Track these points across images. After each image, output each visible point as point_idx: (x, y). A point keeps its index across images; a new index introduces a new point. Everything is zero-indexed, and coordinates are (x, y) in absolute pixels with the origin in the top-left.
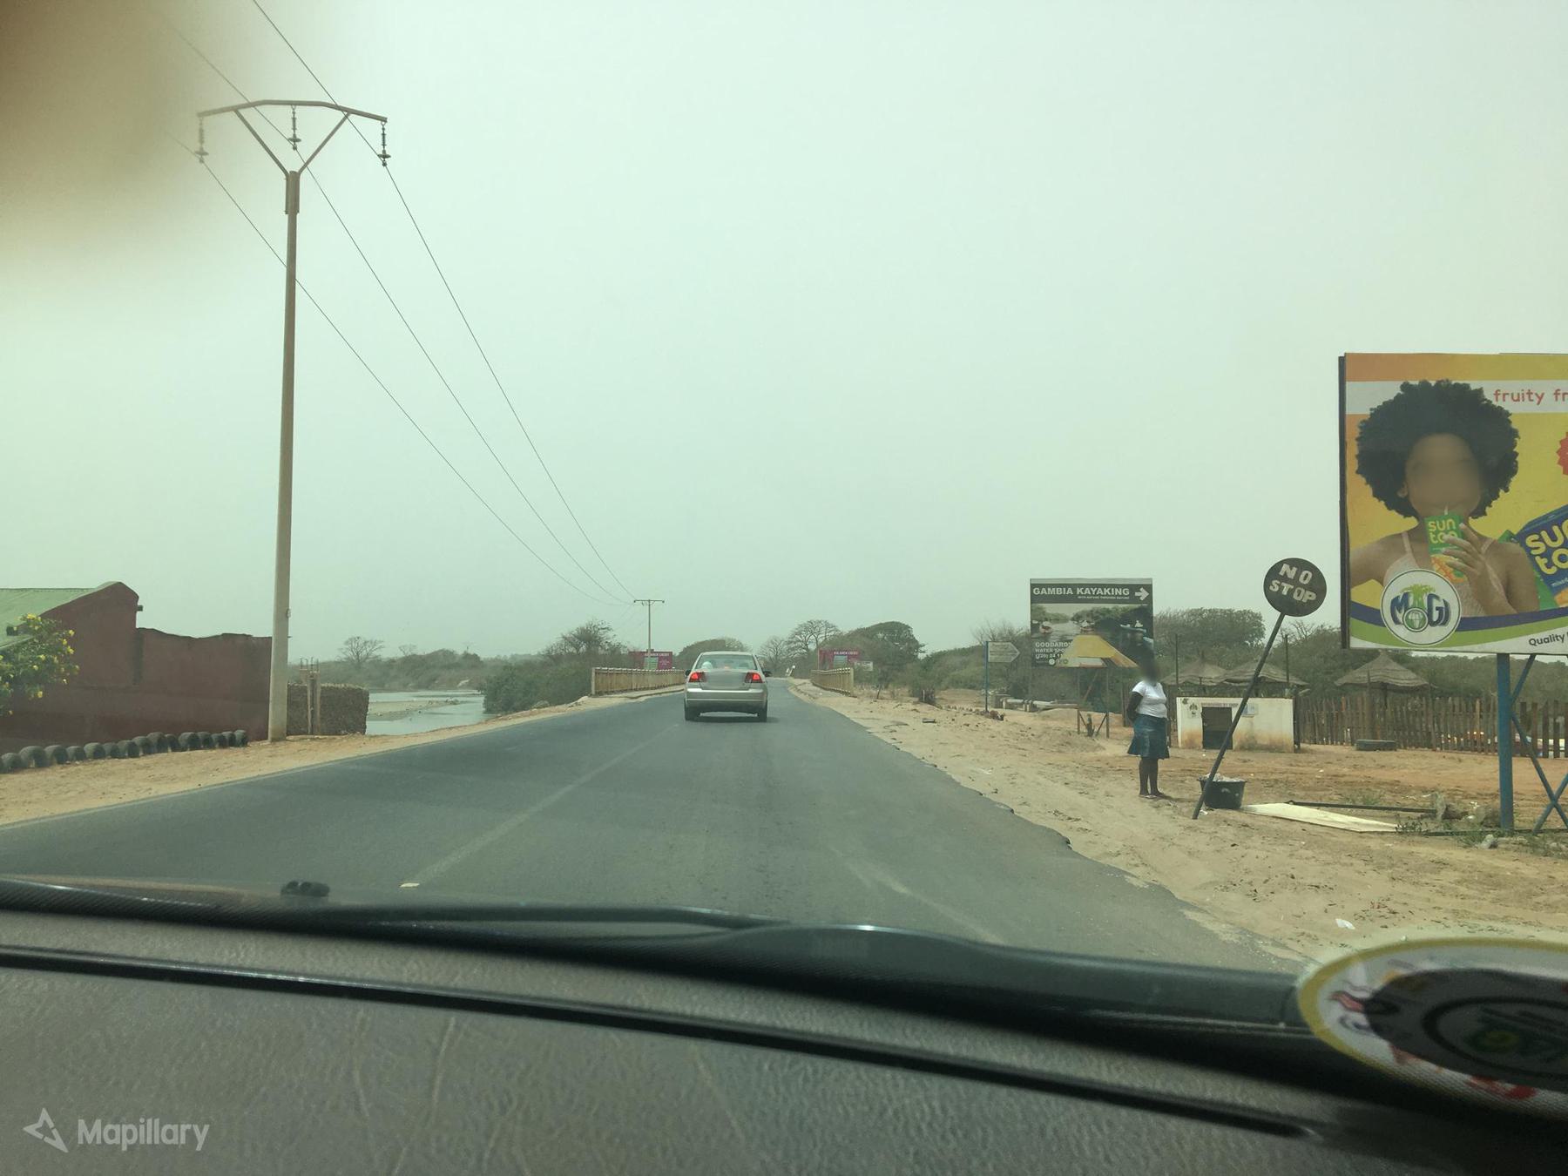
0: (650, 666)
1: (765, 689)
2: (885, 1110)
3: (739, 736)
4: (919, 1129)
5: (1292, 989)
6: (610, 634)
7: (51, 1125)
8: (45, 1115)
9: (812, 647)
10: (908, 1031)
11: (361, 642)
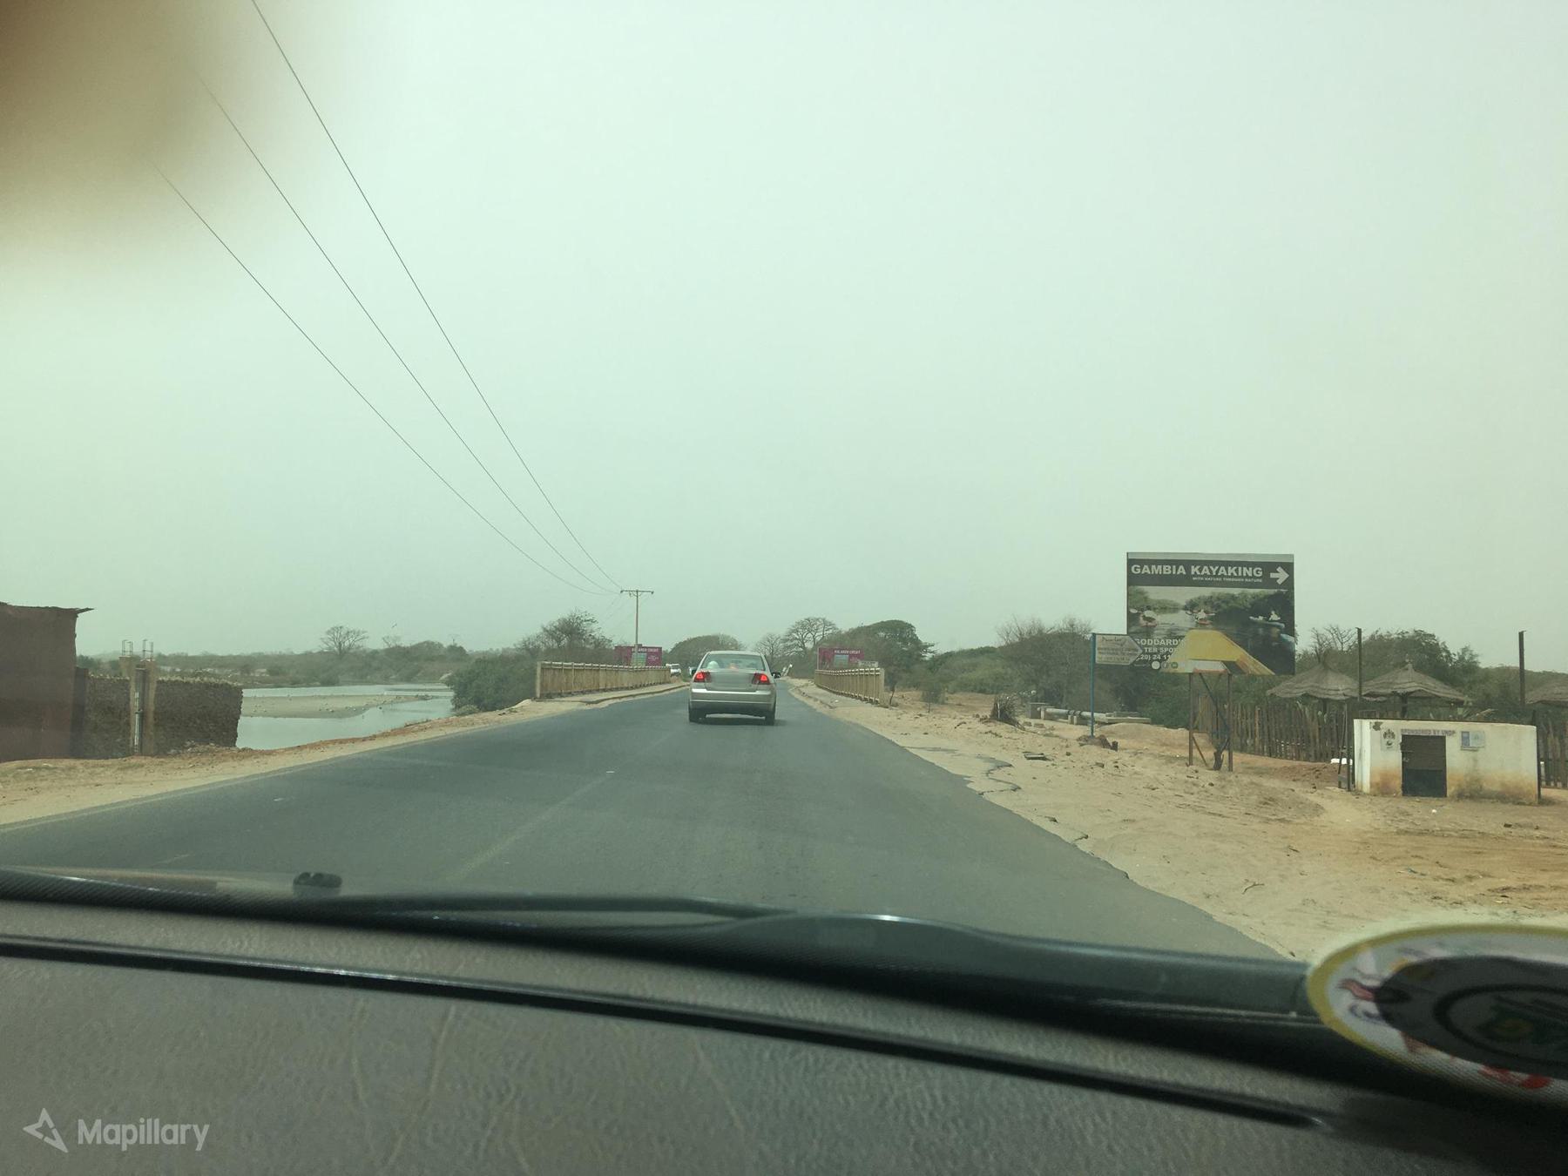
0: (638, 661)
1: (772, 690)
3: (746, 735)
4: (920, 1120)
6: (595, 626)
7: (51, 1125)
8: (45, 1116)
9: (809, 645)
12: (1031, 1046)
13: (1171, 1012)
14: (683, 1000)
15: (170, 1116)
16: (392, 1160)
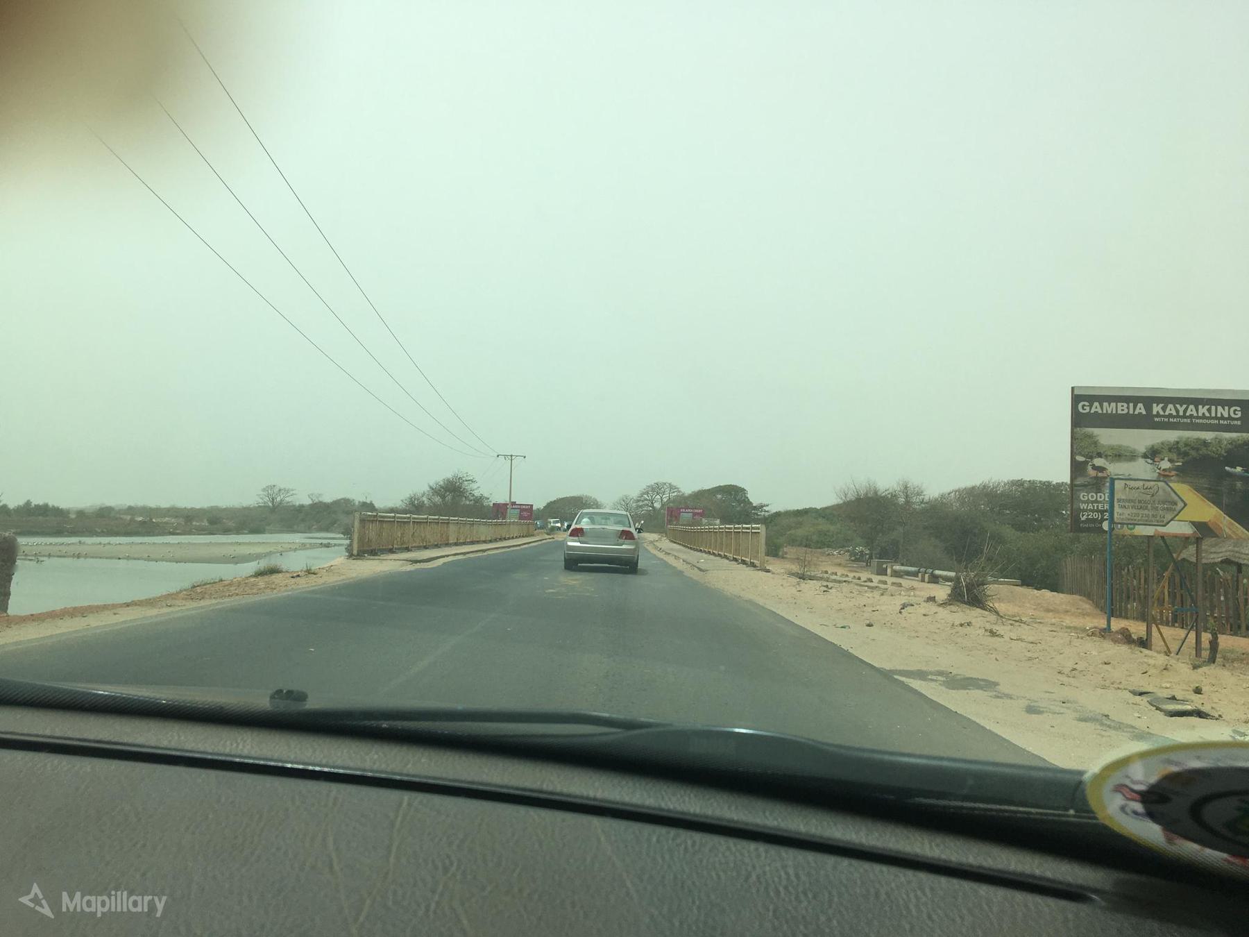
0: (512, 516)
1: (637, 545)
4: (777, 892)
5: (1080, 783)
6: (474, 486)
7: (41, 896)
8: (36, 889)
11: (276, 490)
12: (862, 834)
13: (975, 809)
14: (585, 794)
16: (361, 919)
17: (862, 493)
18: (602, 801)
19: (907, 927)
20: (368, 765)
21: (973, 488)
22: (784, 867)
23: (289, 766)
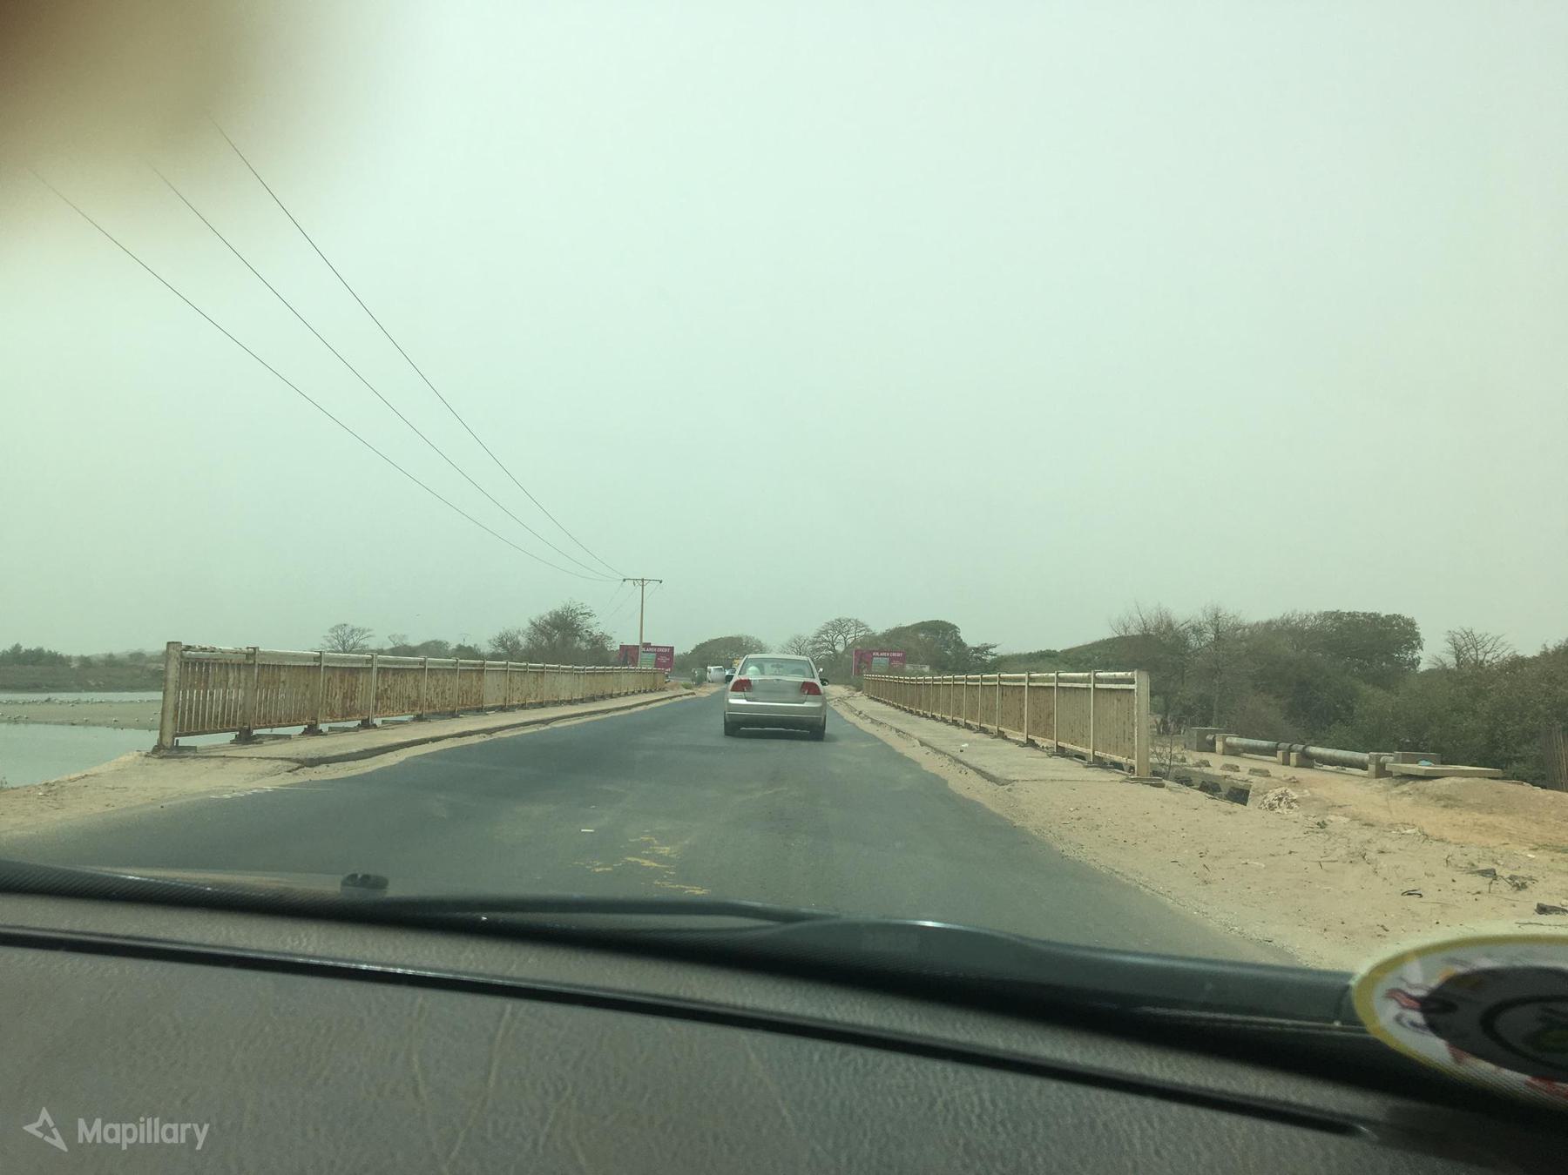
0: (646, 662)
1: (824, 701)
2: (932, 1104)
4: (969, 1122)
5: (1348, 988)
6: (591, 621)
7: (51, 1124)
8: (45, 1115)
9: (840, 648)
10: (958, 1025)
11: (348, 630)
12: (1077, 1051)
15: (103, 1151)
16: (454, 1154)
17: (1152, 624)
18: (752, 1010)
19: (1130, 1165)
20: (462, 966)
21: (1270, 623)
22: (978, 1092)
23: (364, 967)
